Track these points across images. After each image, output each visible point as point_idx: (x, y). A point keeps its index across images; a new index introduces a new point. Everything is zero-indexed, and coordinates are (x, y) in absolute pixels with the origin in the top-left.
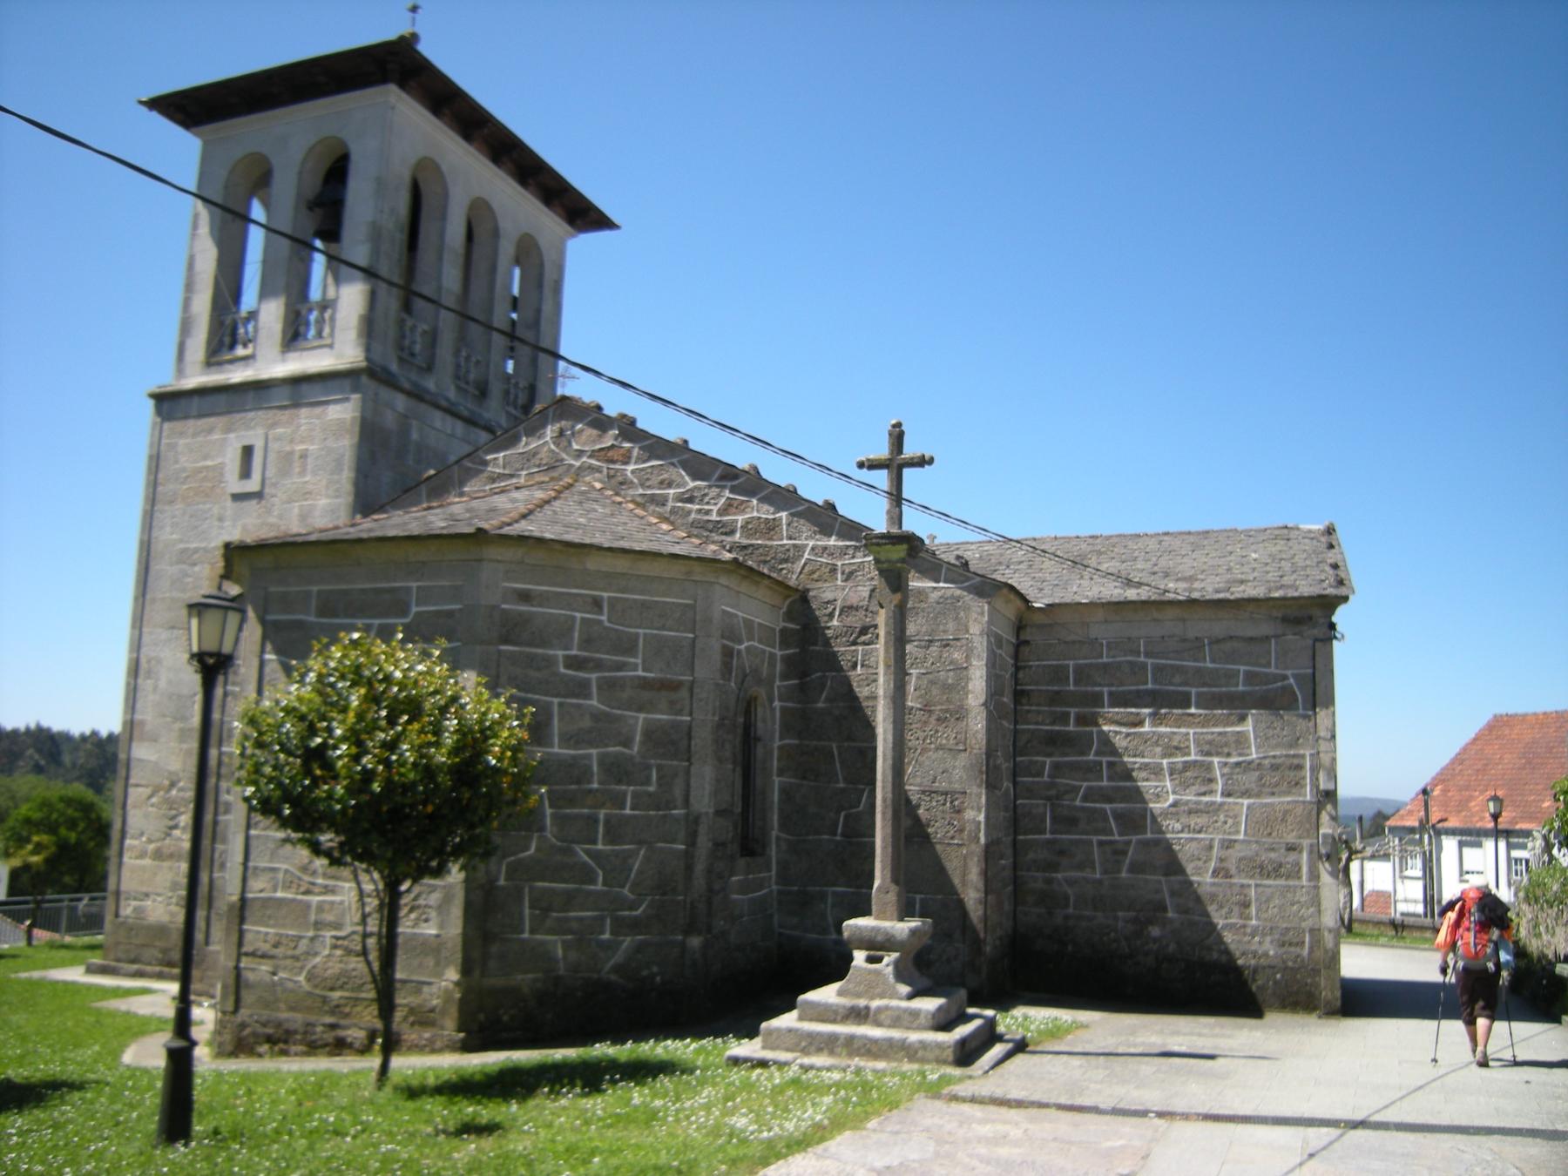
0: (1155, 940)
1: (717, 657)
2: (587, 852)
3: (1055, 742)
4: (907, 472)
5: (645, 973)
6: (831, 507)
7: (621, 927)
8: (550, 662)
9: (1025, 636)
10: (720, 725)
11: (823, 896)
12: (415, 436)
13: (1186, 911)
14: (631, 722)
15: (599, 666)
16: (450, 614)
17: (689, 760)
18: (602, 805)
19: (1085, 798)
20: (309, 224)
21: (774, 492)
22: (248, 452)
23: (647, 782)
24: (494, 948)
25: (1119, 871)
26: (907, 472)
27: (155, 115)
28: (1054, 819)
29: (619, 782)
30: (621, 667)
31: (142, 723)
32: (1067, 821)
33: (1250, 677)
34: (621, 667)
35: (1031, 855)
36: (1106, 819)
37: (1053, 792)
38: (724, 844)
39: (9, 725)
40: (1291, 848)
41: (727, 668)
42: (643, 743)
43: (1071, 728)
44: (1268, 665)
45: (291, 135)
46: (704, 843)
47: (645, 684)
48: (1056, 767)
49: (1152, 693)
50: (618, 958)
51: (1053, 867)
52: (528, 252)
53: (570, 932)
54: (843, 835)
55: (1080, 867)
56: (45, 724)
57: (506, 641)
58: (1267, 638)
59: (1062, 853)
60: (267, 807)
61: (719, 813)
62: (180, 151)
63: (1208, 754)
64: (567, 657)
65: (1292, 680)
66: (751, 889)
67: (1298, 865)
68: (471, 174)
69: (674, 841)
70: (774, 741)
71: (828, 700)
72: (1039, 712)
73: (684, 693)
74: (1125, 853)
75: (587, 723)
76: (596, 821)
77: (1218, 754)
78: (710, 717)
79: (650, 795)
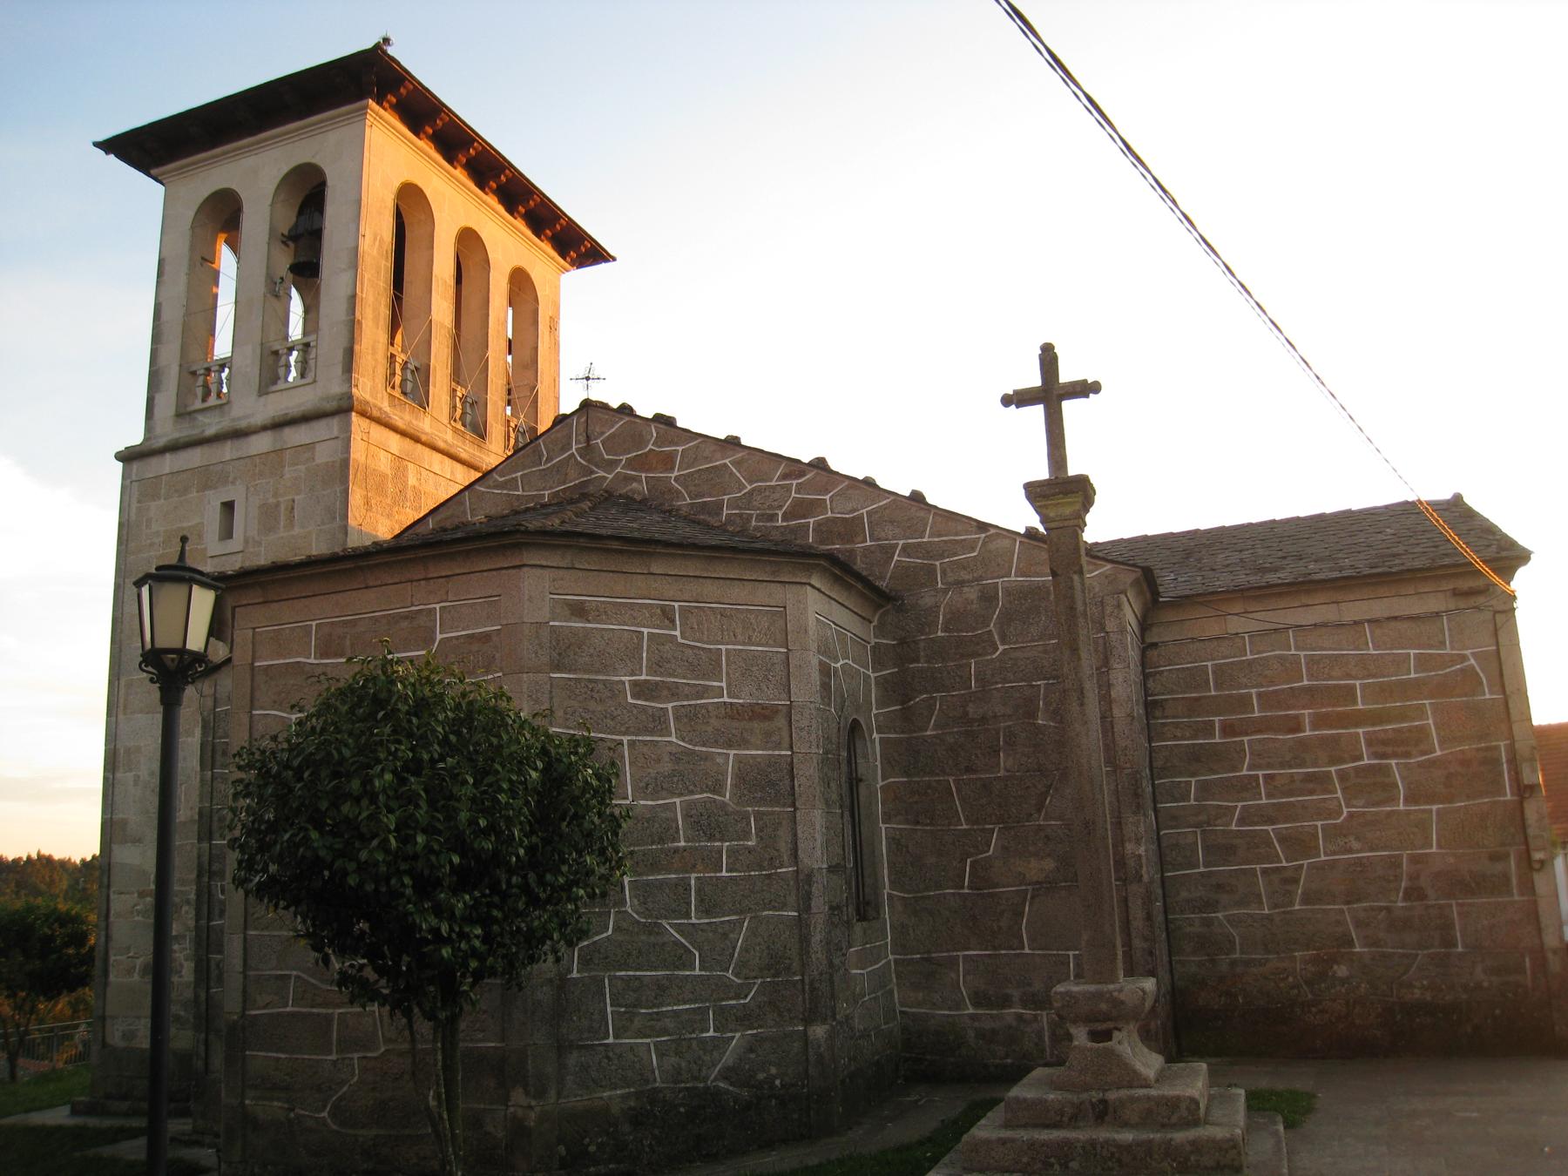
0: (1343, 981)
1: (816, 677)
2: (678, 927)
3: (1197, 758)
4: (1067, 405)
5: (761, 1076)
6: (917, 497)
7: (726, 1019)
8: (614, 691)
9: (1152, 638)
10: (824, 761)
11: (953, 962)
12: (412, 481)
13: (1376, 943)
14: (720, 760)
15: (674, 692)
16: (486, 637)
17: (793, 805)
18: (693, 868)
19: (1242, 821)
20: (284, 260)
21: (848, 487)
22: (229, 507)
23: (746, 835)
24: (572, 1059)
25: (1292, 904)
26: (1067, 405)
27: (112, 159)
28: (1206, 848)
29: (711, 838)
30: (703, 692)
31: (124, 823)
32: (1222, 850)
33: (1208, 729)
34: (703, 692)
35: (1184, 894)
36: (1270, 844)
37: (1203, 818)
38: (838, 907)
39: (10, 856)
40: (1494, 858)
41: (825, 686)
42: (735, 786)
43: (1217, 740)
44: (1442, 644)
45: (257, 171)
46: (819, 905)
47: (733, 712)
48: (1205, 788)
49: (1309, 690)
50: (728, 1058)
51: (1210, 905)
52: (520, 283)
53: (665, 1032)
54: (970, 887)
55: (1241, 903)
56: (46, 852)
57: (558, 668)
58: (1438, 614)
59: (1219, 887)
60: (271, 891)
61: (832, 869)
62: (141, 198)
63: (1384, 756)
64: (635, 684)
65: (1472, 661)
66: (871, 978)
67: (1506, 878)
68: (456, 203)
69: (783, 907)
70: (877, 779)
71: (936, 727)
72: (1177, 725)
73: (781, 722)
74: (1296, 881)
75: (667, 767)
76: (687, 889)
77: (1395, 755)
78: (814, 750)
79: (750, 850)
